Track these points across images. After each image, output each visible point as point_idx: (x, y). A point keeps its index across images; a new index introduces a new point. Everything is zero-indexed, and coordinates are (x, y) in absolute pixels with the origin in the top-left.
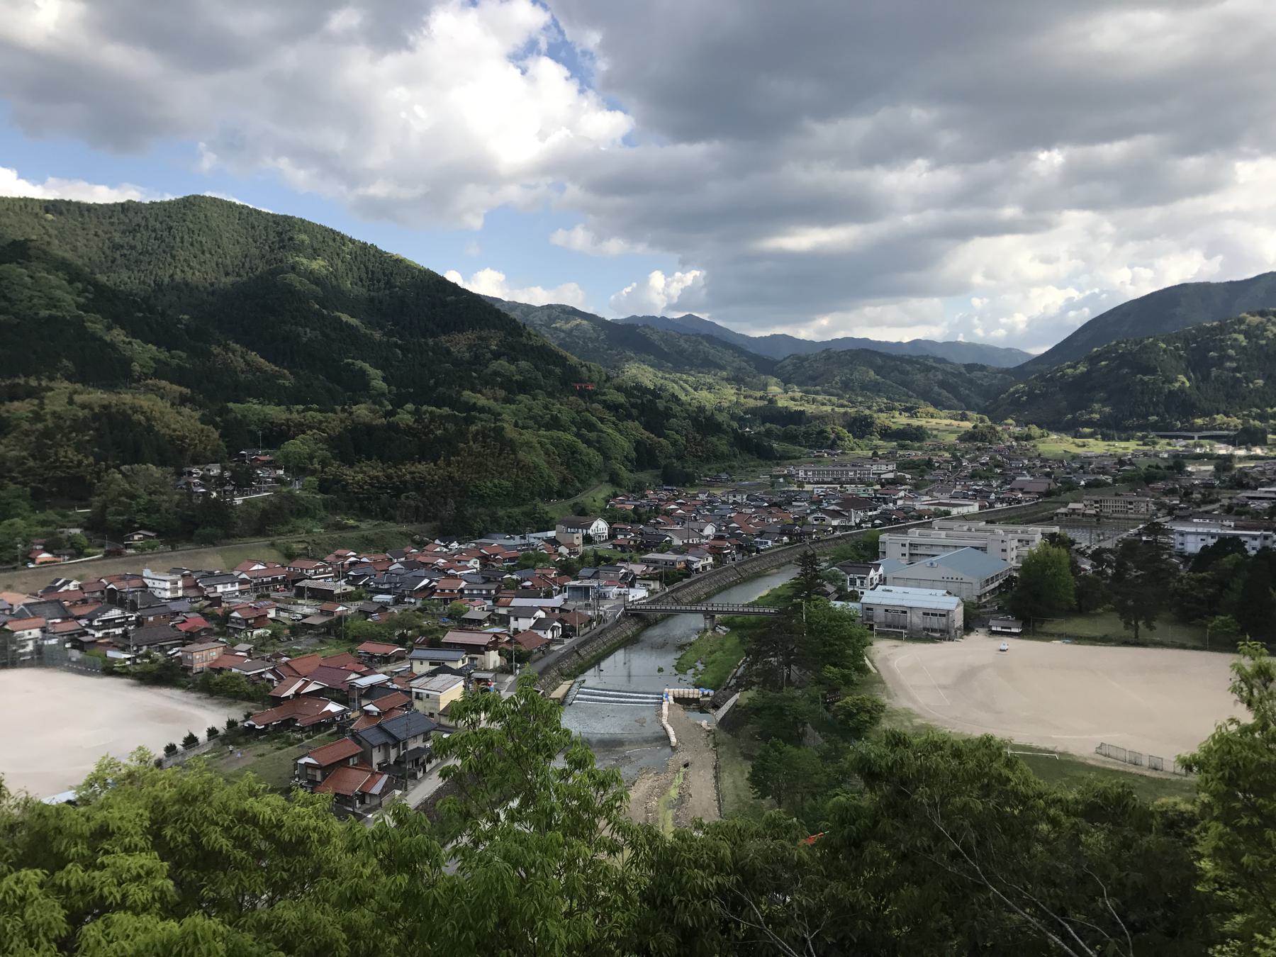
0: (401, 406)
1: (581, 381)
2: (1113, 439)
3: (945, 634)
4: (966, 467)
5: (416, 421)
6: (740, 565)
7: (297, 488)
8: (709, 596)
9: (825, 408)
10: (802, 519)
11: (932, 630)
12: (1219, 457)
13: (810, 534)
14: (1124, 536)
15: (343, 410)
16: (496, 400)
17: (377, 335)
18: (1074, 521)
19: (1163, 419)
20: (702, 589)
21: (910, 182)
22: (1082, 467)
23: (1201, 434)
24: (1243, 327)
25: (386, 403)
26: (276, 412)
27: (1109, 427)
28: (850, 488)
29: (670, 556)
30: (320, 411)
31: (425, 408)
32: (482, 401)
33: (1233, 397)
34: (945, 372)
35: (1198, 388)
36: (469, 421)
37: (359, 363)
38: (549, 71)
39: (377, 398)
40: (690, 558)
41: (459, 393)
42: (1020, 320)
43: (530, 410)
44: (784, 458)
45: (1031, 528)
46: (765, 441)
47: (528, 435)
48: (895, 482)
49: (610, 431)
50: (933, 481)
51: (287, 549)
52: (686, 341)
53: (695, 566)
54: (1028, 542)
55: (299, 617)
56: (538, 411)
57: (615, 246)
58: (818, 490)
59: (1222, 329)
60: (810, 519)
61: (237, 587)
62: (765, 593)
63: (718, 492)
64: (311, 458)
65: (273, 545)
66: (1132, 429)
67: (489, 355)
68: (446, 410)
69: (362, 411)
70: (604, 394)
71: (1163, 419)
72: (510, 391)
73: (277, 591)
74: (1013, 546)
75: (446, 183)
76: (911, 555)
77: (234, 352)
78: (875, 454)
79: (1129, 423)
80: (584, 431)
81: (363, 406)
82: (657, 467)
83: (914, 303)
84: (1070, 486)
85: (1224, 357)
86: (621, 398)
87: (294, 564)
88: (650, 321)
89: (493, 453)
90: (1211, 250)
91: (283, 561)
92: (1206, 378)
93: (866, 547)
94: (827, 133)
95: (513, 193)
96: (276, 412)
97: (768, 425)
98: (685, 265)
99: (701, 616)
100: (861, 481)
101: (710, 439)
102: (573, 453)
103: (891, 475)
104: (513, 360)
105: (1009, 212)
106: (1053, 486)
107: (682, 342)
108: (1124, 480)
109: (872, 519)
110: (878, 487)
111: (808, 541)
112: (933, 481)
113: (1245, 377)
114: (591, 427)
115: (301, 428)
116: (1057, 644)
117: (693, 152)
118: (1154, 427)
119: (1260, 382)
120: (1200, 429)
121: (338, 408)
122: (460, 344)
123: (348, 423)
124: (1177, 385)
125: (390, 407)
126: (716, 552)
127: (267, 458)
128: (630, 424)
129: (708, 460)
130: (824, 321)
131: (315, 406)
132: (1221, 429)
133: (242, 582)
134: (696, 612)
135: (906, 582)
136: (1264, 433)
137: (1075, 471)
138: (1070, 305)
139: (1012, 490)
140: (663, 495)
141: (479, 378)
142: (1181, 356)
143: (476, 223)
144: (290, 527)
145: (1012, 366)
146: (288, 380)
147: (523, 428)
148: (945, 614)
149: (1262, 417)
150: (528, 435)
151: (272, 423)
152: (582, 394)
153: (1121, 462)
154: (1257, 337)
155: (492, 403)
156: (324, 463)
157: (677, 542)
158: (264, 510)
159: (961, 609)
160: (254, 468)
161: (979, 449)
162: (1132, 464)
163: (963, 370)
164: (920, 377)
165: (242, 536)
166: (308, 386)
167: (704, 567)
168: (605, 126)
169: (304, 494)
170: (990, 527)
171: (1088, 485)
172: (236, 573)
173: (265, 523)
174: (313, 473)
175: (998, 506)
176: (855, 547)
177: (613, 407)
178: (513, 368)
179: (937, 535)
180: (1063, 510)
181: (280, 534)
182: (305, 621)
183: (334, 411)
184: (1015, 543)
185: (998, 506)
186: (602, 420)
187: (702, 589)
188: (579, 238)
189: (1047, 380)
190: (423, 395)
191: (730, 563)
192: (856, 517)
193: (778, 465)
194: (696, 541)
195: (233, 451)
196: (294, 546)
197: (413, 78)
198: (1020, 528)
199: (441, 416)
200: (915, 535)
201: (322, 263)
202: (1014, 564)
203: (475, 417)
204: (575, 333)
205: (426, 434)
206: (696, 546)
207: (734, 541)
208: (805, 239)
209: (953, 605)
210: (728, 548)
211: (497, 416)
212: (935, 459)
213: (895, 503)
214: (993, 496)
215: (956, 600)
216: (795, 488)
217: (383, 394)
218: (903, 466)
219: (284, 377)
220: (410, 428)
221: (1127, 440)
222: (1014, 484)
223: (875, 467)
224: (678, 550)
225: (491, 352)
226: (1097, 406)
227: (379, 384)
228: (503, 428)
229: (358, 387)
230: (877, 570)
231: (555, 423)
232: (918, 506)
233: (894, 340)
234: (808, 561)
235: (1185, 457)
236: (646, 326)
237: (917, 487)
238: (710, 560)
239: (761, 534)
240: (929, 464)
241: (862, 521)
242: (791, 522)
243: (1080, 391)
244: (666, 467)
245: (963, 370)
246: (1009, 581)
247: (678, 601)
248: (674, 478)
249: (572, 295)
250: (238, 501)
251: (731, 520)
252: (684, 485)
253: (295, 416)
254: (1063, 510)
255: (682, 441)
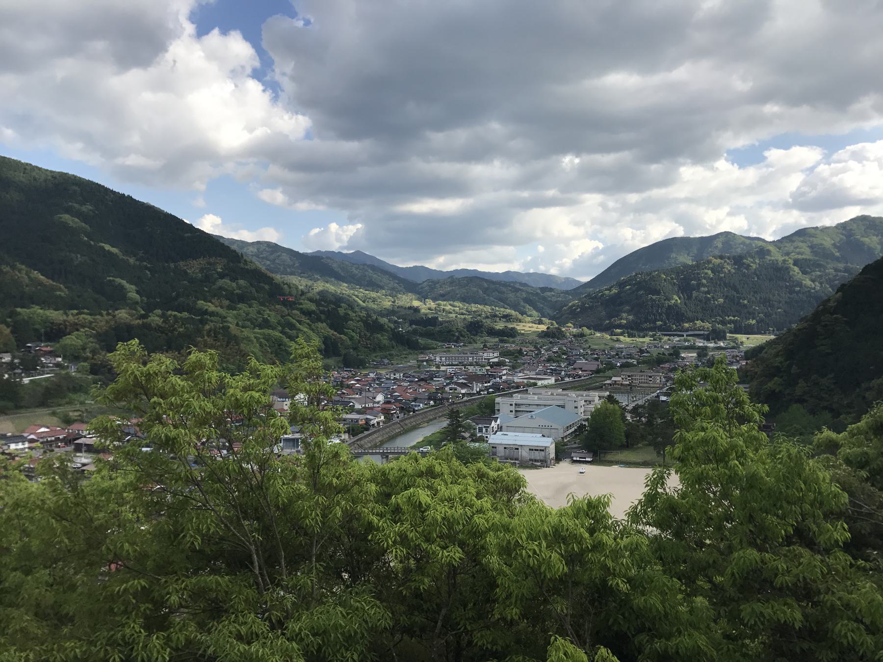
0: (152, 311)
1: (283, 294)
2: (635, 336)
3: (544, 463)
4: (544, 355)
5: (164, 322)
6: (401, 421)
7: (73, 371)
8: (382, 443)
9: (451, 315)
10: (442, 389)
11: (538, 461)
12: (699, 348)
13: (448, 399)
14: (649, 397)
15: (108, 314)
16: (222, 307)
17: (132, 261)
18: (616, 388)
19: (665, 324)
20: (377, 438)
21: (492, 172)
22: (617, 354)
23: (690, 333)
24: (711, 266)
25: (139, 309)
26: (56, 315)
27: (632, 329)
28: (471, 369)
29: (354, 416)
30: (91, 315)
31: (170, 312)
32: (211, 308)
33: (707, 310)
34: (527, 292)
35: (685, 304)
36: (203, 322)
37: (118, 280)
38: (254, 87)
39: (133, 305)
40: (368, 417)
41: (195, 302)
42: (567, 262)
43: (247, 314)
44: (425, 349)
45: (592, 393)
46: (417, 335)
47: (246, 332)
48: (499, 364)
49: (305, 330)
50: (524, 364)
51: (66, 416)
52: (357, 269)
53: (372, 423)
54: (590, 402)
55: (79, 465)
56: (253, 315)
57: (303, 206)
58: (450, 370)
59: (698, 266)
60: (447, 389)
61: (27, 445)
62: (421, 439)
63: (383, 372)
64: (84, 349)
65: (54, 414)
66: (646, 330)
67: (216, 276)
68: (185, 314)
69: (123, 314)
70: (301, 304)
71: (665, 324)
72: (231, 301)
73: (59, 447)
74: (583, 405)
75: (185, 157)
76: (516, 411)
77: (20, 271)
78: (485, 346)
79: (645, 325)
80: (287, 330)
81: (123, 311)
82: (340, 355)
83: (498, 249)
84: (611, 366)
85: (700, 285)
86: (313, 307)
87: (71, 427)
88: (331, 255)
89: (222, 345)
90: (679, 219)
91: (63, 426)
92: (690, 297)
93: (487, 407)
94: (438, 138)
95: (230, 166)
96: (56, 315)
97: (414, 326)
98: (352, 220)
99: (379, 456)
100: (477, 364)
101: (376, 335)
102: (280, 345)
103: (496, 360)
104: (233, 279)
105: (551, 193)
106: (601, 367)
107: (354, 269)
108: (644, 362)
109: (487, 388)
110: (489, 368)
111: (446, 404)
112: (524, 364)
113: (713, 297)
114: (292, 327)
115: (76, 327)
116: (615, 468)
117: (351, 147)
118: (660, 329)
119: (721, 300)
120: (687, 330)
121: (104, 313)
122: (194, 267)
123: (112, 323)
124: (673, 302)
125: (143, 312)
126: (386, 412)
127: (49, 349)
128: (320, 325)
129: (374, 350)
130: (441, 259)
131: (86, 311)
132: (700, 330)
133: (32, 441)
134: (376, 453)
135: (515, 429)
136: (725, 333)
137: (613, 357)
138: (597, 253)
139: (575, 369)
140: (345, 374)
141: (209, 291)
142: (674, 284)
143: (201, 187)
144: (67, 400)
145: (569, 289)
146: (62, 292)
147: (243, 327)
148: (543, 450)
149: (723, 323)
150: (246, 332)
151: (52, 323)
152: (285, 303)
153: (641, 351)
154: (719, 272)
155: (219, 309)
156: (94, 352)
157: (358, 406)
158: (47, 388)
159: (554, 445)
160: (39, 357)
161: (551, 343)
162: (648, 352)
163: (539, 291)
164: (511, 296)
165: (27, 407)
166: (79, 297)
167: (378, 423)
168: (293, 125)
169: (79, 375)
170: (565, 392)
171: (622, 366)
172: (25, 435)
173: (48, 397)
174: (86, 359)
175: (567, 379)
176: (479, 407)
177: (308, 313)
178: (234, 284)
179: (532, 398)
180: (608, 382)
181: (60, 405)
182: (84, 468)
183: (102, 315)
184: (583, 403)
185: (567, 379)
186: (300, 322)
187: (377, 438)
188: (278, 197)
189: (592, 298)
190: (167, 304)
191: (395, 420)
192: (477, 387)
193: (422, 353)
194: (371, 405)
195: (21, 343)
196: (71, 414)
197: (162, 85)
198: (585, 393)
199: (181, 318)
200: (517, 398)
201: (90, 207)
202: (583, 416)
203: (207, 320)
204: (277, 261)
205: (172, 331)
206: (372, 408)
207: (398, 404)
208: (424, 206)
209: (549, 443)
210: (394, 409)
211: (223, 318)
212: (524, 349)
213: (501, 377)
214: (563, 373)
215: (550, 440)
216: (434, 369)
217: (137, 303)
218: (502, 354)
219: (60, 290)
220: (160, 327)
221: (644, 337)
222: (575, 366)
223: (485, 355)
224: (359, 412)
225: (218, 273)
226: (624, 315)
227: (133, 295)
228: (229, 327)
229: (118, 298)
230: (496, 421)
231: (266, 324)
232: (516, 380)
233: (486, 270)
234: (454, 415)
235: (680, 348)
236: (328, 258)
237: (513, 368)
238: (382, 418)
239: (415, 400)
240: (520, 352)
241: (481, 390)
242: (434, 391)
243: (613, 304)
244: (345, 355)
245: (539, 291)
246: (581, 428)
247: (361, 447)
248: (351, 363)
249: (271, 235)
250: (26, 380)
251: (394, 391)
252: (358, 368)
253: (71, 317)
254: (608, 382)
255: (356, 337)
